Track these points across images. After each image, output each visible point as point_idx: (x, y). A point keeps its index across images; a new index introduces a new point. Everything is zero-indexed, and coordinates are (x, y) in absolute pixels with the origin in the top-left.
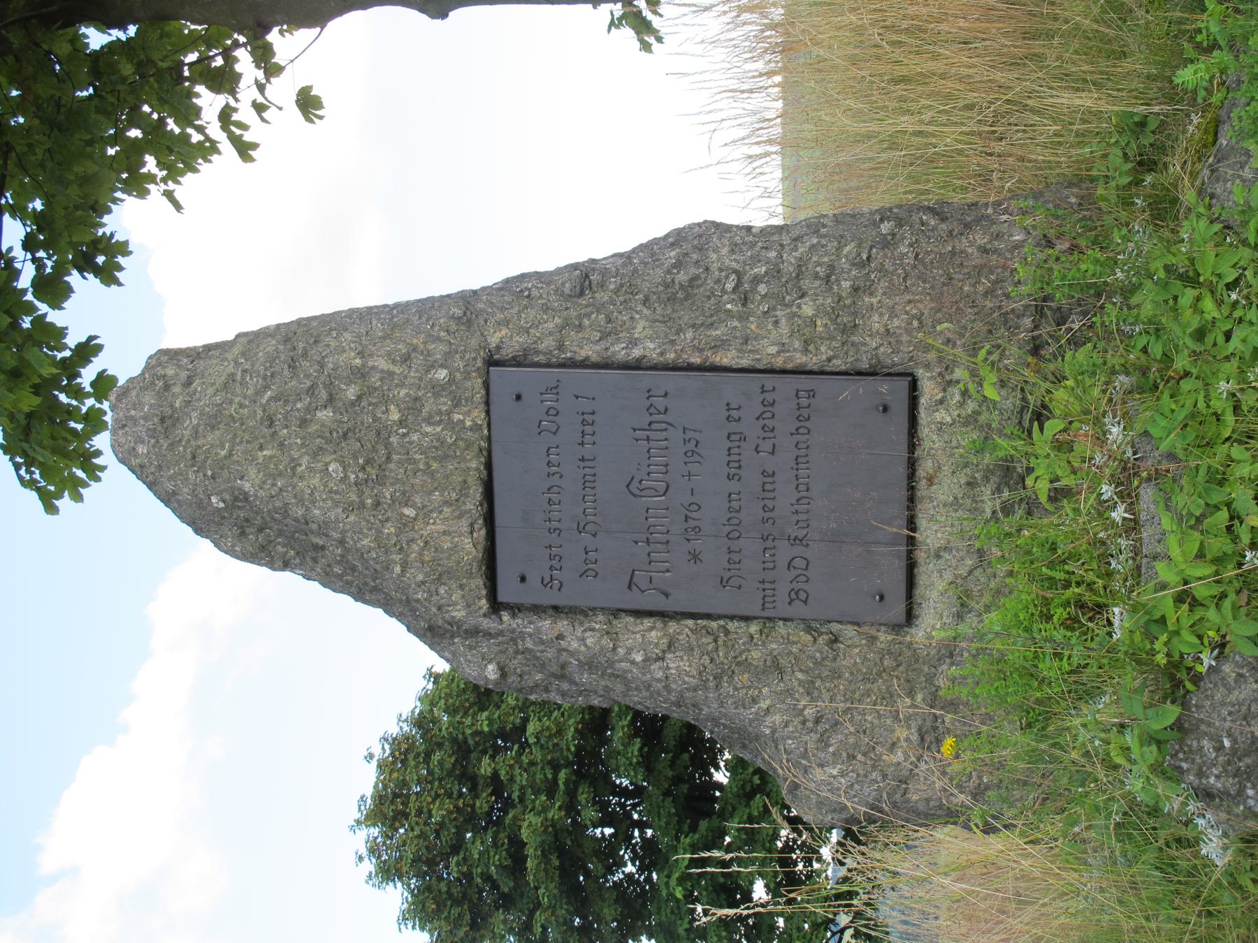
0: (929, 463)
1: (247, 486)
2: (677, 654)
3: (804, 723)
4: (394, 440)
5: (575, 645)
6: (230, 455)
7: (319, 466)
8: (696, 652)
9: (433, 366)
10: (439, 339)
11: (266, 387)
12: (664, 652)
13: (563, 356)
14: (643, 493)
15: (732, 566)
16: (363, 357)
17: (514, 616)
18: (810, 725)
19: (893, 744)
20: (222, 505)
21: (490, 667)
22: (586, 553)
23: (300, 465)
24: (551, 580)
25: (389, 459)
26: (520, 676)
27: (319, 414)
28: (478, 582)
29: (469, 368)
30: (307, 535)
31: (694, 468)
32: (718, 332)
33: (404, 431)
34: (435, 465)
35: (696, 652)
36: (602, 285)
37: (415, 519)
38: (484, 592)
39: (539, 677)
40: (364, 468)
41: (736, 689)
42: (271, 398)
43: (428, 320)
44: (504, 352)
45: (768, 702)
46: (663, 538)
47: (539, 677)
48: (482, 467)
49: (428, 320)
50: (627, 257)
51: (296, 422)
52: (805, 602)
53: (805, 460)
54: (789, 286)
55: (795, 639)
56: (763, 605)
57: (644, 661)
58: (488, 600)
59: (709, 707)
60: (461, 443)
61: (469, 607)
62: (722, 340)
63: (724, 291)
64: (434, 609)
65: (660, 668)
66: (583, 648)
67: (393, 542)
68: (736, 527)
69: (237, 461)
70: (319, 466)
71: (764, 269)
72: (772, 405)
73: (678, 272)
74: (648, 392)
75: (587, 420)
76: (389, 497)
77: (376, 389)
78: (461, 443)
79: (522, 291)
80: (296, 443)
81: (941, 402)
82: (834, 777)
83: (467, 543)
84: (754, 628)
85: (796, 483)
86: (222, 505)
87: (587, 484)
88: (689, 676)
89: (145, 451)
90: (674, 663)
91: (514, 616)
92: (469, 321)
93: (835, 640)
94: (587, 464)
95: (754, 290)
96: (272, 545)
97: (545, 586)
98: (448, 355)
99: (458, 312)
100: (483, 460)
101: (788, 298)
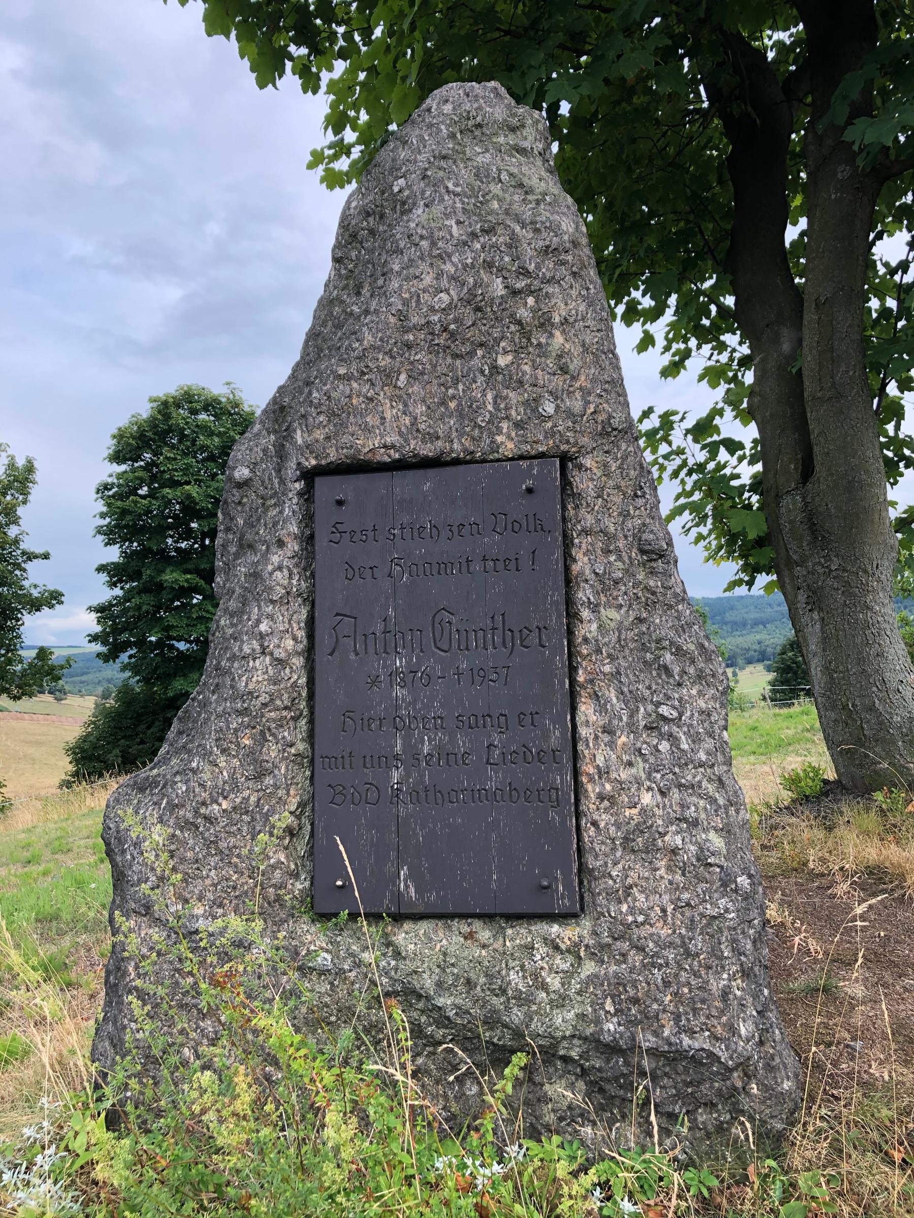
3: (204, 803)
7: (444, 283)
9: (556, 398)
14: (437, 626)
15: (366, 723)
16: (562, 324)
20: (396, 189)
22: (371, 568)
25: (456, 356)
28: (333, 455)
33: (487, 372)
36: (653, 573)
37: (395, 387)
38: (323, 462)
40: (445, 330)
41: (236, 730)
43: (605, 390)
49: (605, 390)
54: (671, 776)
57: (261, 633)
58: (315, 467)
60: (477, 432)
63: (658, 704)
65: (254, 650)
66: (270, 568)
67: (370, 364)
76: (417, 358)
77: (529, 340)
81: (557, 948)
91: (300, 494)
96: (358, 245)
98: (570, 414)
101: (658, 776)
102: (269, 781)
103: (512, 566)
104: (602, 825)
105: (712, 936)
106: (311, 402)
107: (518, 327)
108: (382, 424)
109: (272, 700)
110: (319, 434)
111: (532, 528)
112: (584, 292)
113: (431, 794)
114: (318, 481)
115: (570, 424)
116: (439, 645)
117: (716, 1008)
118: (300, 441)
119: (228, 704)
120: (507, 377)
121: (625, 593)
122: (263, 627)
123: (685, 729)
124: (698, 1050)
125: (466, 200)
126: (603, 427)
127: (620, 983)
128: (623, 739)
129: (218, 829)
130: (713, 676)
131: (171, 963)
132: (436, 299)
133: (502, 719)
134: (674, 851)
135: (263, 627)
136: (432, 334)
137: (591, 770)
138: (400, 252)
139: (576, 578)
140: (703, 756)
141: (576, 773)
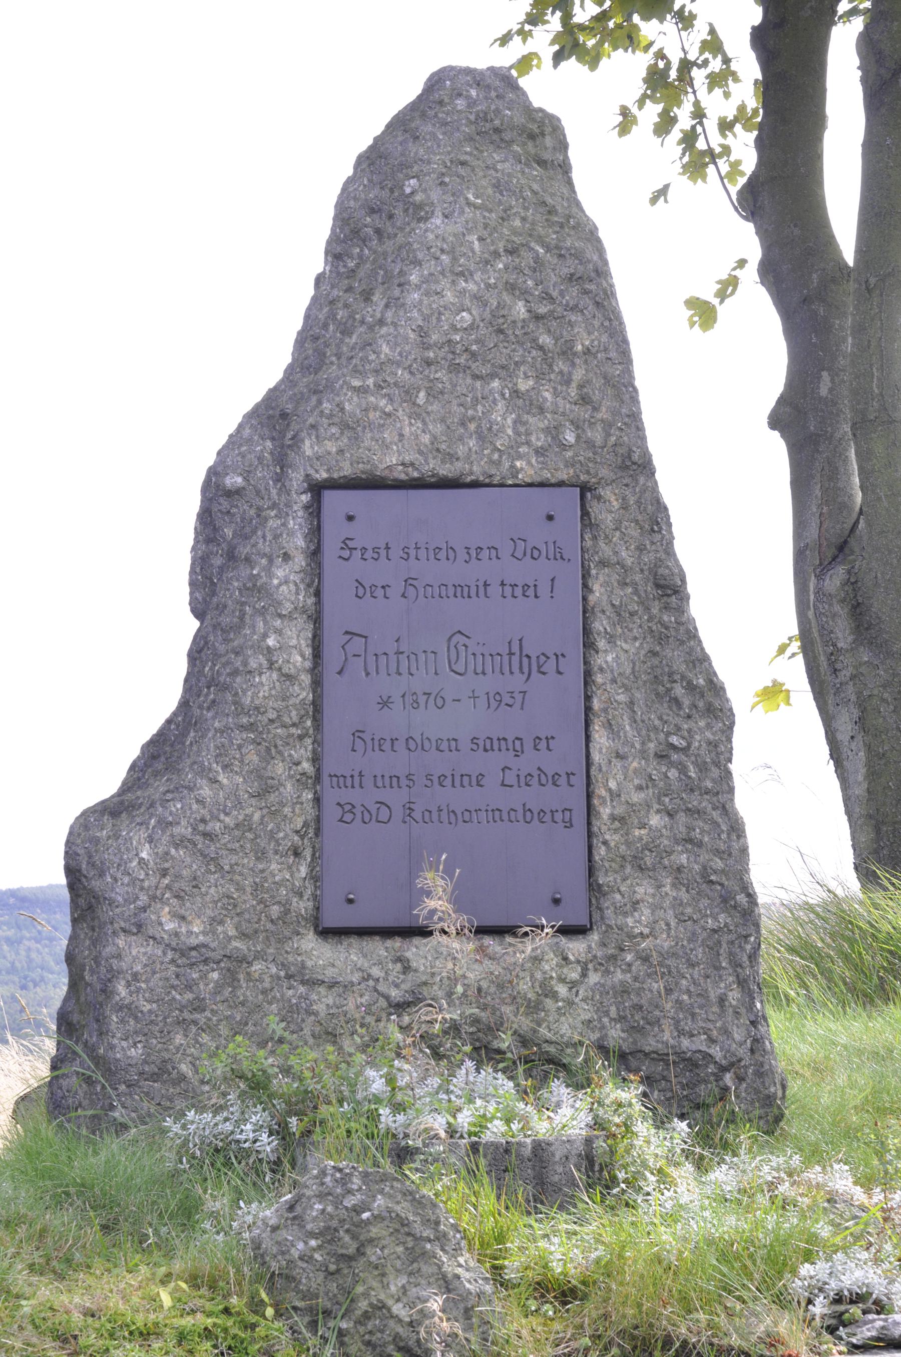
0: (498, 949)
1: (437, 221)
2: (277, 684)
3: (203, 821)
4: (496, 384)
5: (280, 573)
6: (469, 204)
7: (467, 302)
8: (280, 704)
9: (577, 428)
10: (608, 435)
11: (548, 249)
12: (280, 669)
13: (592, 566)
14: (452, 649)
15: (376, 743)
16: (585, 354)
17: (306, 507)
18: (201, 827)
19: (183, 918)
20: (408, 190)
21: (239, 480)
22: (383, 587)
23: (466, 281)
24: (350, 549)
25: (476, 377)
26: (229, 512)
27: (521, 304)
28: (347, 470)
29: (578, 466)
30: (383, 283)
31: (482, 702)
32: (628, 728)
33: (507, 395)
34: (472, 427)
35: (280, 704)
36: (666, 608)
37: (414, 404)
38: (336, 476)
39: (228, 532)
40: (466, 350)
41: (240, 747)
42: (537, 253)
43: (625, 424)
44: (595, 503)
45: (225, 781)
46: (404, 669)
47: (228, 532)
48: (473, 477)
49: (625, 424)
50: (693, 635)
51: (512, 278)
52: (341, 820)
53: (497, 818)
54: (678, 801)
55: (297, 810)
56: (336, 776)
57: (268, 648)
58: (326, 480)
59: (214, 718)
60: (496, 456)
61: (317, 459)
62: (619, 732)
63: (668, 734)
64: (311, 420)
65: (261, 665)
66: (276, 582)
67: (388, 379)
68: (420, 747)
69: (463, 212)
70: (467, 302)
71: (693, 775)
72: (555, 784)
73: (683, 687)
74: (563, 655)
75: (529, 590)
76: (437, 376)
77: (551, 366)
78: (496, 456)
79: (658, 524)
80: (489, 278)
81: (565, 959)
82: (137, 855)
83: (393, 459)
84: (306, 766)
85: (472, 810)
86: (408, 190)
87: (459, 589)
88: (252, 698)
89: (459, 108)
90: (268, 680)
91: (306, 507)
92: (627, 467)
93: (297, 854)
94: (481, 589)
95: (671, 764)
96: (360, 243)
97: (344, 542)
98: (590, 444)
99: (635, 457)
100: (481, 478)
101: (667, 800)
102: (273, 798)
103: (531, 592)
104: (612, 844)
105: (712, 949)
106: (322, 412)
107: (540, 353)
108: (400, 441)
109: (279, 716)
110: (331, 447)
111: (551, 556)
112: (607, 323)
113: (444, 814)
114: (329, 496)
115: (591, 455)
116: (454, 667)
117: (714, 1013)
118: (309, 452)
119: (230, 720)
120: (527, 403)
121: (640, 626)
122: (271, 642)
123: (693, 758)
124: (695, 1052)
125: (487, 215)
126: (623, 461)
127: (624, 991)
128: (635, 764)
129: (218, 845)
130: (721, 710)
131: (167, 979)
132: (458, 318)
133: (518, 743)
134: (679, 869)
135: (271, 642)
136: (453, 353)
137: (603, 792)
138: (417, 263)
139: (593, 608)
140: (709, 784)
141: (589, 796)
